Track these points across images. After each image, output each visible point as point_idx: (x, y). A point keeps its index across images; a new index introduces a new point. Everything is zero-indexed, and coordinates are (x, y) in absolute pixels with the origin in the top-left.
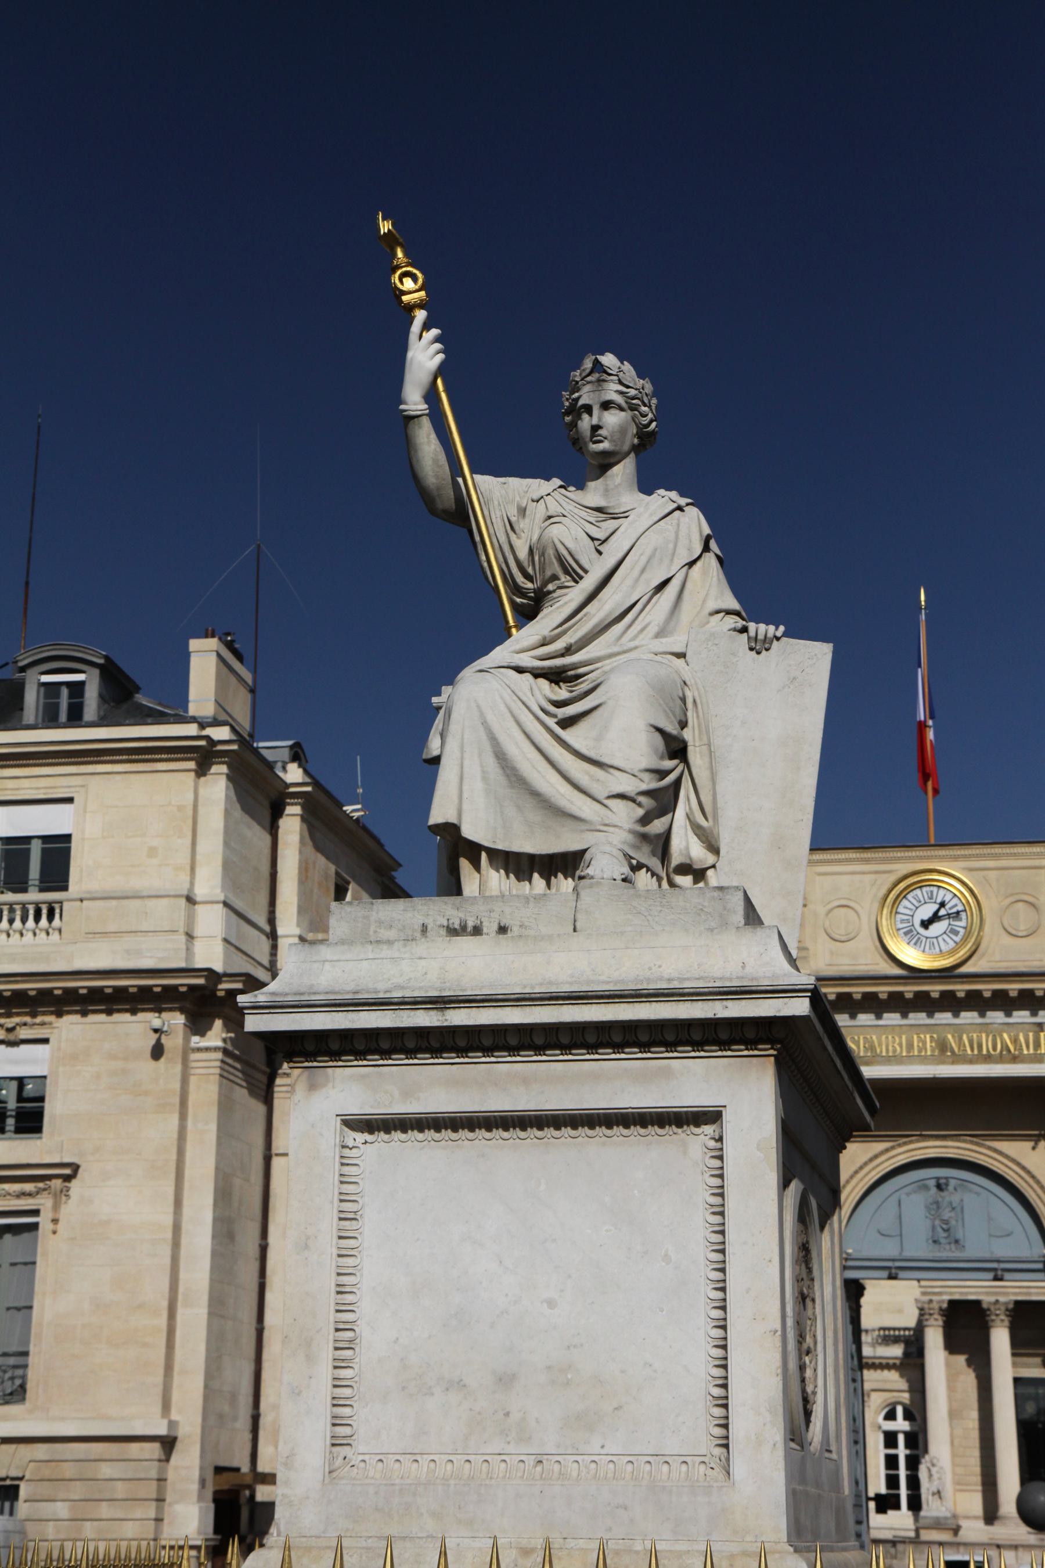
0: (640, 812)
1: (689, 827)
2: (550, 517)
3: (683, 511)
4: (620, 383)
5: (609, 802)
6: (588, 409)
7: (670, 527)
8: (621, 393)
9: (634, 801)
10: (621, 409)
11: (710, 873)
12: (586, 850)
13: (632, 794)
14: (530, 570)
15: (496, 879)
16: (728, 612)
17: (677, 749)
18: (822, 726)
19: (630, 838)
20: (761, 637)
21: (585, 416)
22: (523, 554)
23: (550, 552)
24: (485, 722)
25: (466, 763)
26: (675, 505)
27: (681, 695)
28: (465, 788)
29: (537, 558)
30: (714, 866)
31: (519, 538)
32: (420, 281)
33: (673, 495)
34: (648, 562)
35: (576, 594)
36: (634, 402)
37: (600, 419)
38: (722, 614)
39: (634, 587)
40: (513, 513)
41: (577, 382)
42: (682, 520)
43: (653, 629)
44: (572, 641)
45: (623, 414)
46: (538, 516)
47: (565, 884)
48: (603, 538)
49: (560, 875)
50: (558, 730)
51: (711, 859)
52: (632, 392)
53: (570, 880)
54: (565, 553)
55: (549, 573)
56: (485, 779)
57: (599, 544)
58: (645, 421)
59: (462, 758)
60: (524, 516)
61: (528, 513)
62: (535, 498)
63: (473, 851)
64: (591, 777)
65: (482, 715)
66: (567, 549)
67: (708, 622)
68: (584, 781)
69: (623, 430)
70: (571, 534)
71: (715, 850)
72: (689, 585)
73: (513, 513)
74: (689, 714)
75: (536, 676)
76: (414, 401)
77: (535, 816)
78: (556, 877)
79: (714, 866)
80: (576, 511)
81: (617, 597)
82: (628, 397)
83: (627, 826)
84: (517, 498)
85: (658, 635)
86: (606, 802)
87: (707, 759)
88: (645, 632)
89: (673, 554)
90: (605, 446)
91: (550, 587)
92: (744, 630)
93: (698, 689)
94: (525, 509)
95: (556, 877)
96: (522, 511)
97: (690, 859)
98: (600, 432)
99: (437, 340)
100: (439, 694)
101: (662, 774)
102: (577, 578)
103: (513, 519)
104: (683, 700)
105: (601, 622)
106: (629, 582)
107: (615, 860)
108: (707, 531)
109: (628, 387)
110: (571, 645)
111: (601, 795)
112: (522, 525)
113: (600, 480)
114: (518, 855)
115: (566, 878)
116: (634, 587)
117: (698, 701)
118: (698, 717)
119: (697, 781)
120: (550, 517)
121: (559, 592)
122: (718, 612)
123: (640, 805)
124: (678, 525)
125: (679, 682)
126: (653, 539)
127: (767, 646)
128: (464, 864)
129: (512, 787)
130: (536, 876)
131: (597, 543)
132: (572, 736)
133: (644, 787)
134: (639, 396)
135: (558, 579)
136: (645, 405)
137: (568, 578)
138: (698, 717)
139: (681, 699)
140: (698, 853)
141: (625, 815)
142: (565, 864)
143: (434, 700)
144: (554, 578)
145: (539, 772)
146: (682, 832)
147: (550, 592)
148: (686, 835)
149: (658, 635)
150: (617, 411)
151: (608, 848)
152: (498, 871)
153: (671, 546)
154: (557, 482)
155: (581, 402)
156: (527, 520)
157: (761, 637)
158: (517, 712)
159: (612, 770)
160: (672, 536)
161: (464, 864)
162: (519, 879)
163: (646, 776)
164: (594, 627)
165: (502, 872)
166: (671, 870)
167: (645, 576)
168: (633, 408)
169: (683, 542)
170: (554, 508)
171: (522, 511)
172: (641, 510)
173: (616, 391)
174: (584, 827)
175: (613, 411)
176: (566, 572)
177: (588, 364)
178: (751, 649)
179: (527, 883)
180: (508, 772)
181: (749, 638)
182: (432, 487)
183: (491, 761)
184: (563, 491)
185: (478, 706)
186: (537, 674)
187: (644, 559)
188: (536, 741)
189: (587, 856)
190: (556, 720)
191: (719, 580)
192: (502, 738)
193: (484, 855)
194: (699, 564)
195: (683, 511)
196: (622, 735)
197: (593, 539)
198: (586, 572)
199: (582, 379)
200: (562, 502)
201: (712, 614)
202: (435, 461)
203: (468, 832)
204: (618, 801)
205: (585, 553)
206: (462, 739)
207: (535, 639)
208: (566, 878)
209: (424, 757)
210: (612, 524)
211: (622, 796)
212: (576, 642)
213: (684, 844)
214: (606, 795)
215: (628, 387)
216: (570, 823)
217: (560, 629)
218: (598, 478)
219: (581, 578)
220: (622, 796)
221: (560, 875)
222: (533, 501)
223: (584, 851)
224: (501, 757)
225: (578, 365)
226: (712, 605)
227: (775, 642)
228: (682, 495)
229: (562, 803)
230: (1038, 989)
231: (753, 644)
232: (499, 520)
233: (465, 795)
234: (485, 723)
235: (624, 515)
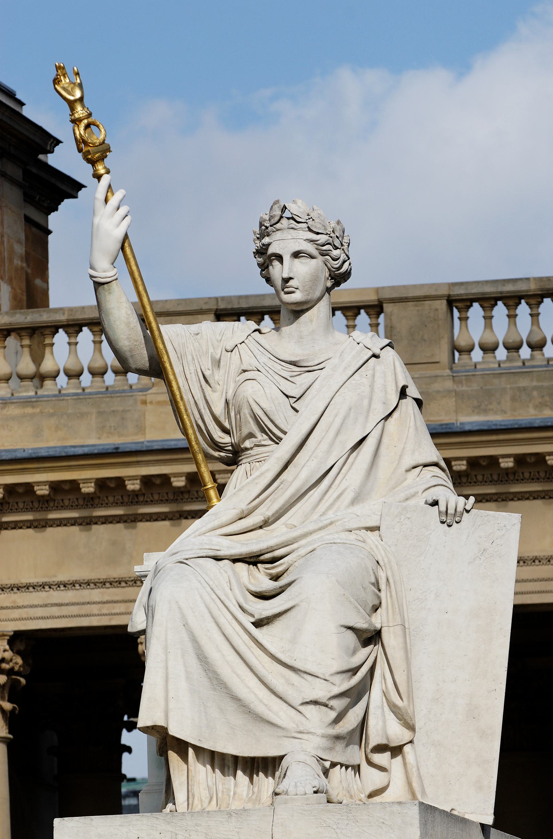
0: (333, 715)
1: (385, 704)
2: (245, 371)
4: (310, 230)
5: (301, 708)
9: (326, 706)
10: (312, 257)
11: (407, 749)
13: (324, 700)
14: (227, 425)
15: (202, 772)
17: (371, 638)
19: (324, 742)
20: (451, 511)
21: (276, 263)
22: (219, 409)
23: (246, 411)
24: (187, 624)
25: (170, 663)
26: (370, 353)
28: (171, 687)
29: (232, 414)
30: (411, 742)
31: (214, 391)
34: (342, 424)
36: (324, 248)
37: (290, 270)
38: (421, 467)
39: (329, 452)
40: (207, 366)
41: (267, 228)
42: (378, 368)
43: (349, 496)
46: (233, 367)
47: (265, 783)
48: (298, 397)
49: (261, 774)
50: (252, 628)
51: (406, 735)
52: (323, 239)
53: (270, 778)
55: (245, 432)
56: (188, 678)
57: (294, 401)
58: (336, 264)
59: (166, 661)
60: (219, 366)
61: (222, 364)
62: (229, 348)
63: (181, 747)
65: (183, 617)
67: (405, 479)
68: (280, 687)
69: (314, 279)
70: (264, 394)
71: (412, 728)
72: (385, 440)
73: (207, 366)
74: (383, 595)
77: (237, 719)
78: (258, 775)
79: (411, 742)
80: (270, 364)
81: (313, 464)
83: (320, 731)
84: (211, 350)
85: (354, 501)
86: (301, 708)
87: (401, 640)
88: (341, 499)
89: (368, 411)
90: (297, 297)
93: (391, 568)
95: (258, 775)
96: (217, 363)
97: (388, 739)
98: (291, 283)
100: (141, 563)
101: (354, 671)
102: (277, 440)
103: (207, 373)
105: (298, 491)
106: (324, 446)
107: (309, 769)
109: (318, 233)
110: (269, 519)
111: (296, 702)
112: (216, 377)
113: (294, 325)
114: (223, 756)
116: (329, 452)
117: (391, 581)
118: (391, 596)
119: (391, 662)
120: (245, 371)
121: (257, 450)
123: (331, 708)
124: (373, 376)
125: (371, 565)
126: (347, 397)
127: (457, 519)
128: (173, 756)
129: (215, 690)
130: (239, 773)
133: (337, 690)
134: (331, 241)
135: (255, 437)
136: (336, 248)
137: (265, 437)
138: (391, 596)
139: (373, 584)
140: (396, 733)
141: (317, 720)
142: (268, 765)
144: (251, 435)
145: (238, 675)
146: (379, 712)
147: (247, 449)
148: (383, 715)
149: (354, 501)
150: (309, 260)
151: (302, 757)
152: (205, 766)
153: (366, 402)
155: (271, 250)
156: (222, 371)
157: (451, 511)
158: (212, 606)
159: (305, 676)
161: (173, 756)
162: (223, 773)
163: (337, 679)
164: (291, 497)
165: (209, 767)
166: (368, 751)
167: (341, 438)
168: (323, 254)
169: (378, 395)
170: (249, 361)
171: (217, 363)
172: (334, 361)
174: (281, 733)
175: (303, 260)
176: (263, 431)
178: (443, 522)
179: (232, 778)
180: (210, 675)
181: (440, 512)
182: (125, 349)
183: (193, 662)
185: (179, 608)
188: (235, 645)
189: (284, 763)
191: (416, 429)
192: (204, 642)
194: (396, 415)
196: (316, 638)
198: (285, 433)
199: (271, 226)
200: (256, 352)
201: (408, 471)
202: (128, 324)
203: (174, 731)
204: (311, 707)
205: (281, 414)
206: (166, 640)
207: (233, 513)
208: (267, 777)
210: (307, 378)
211: (315, 703)
212: (273, 515)
213: (384, 727)
214: (300, 702)
215: (318, 233)
216: (267, 727)
217: (257, 501)
218: (292, 324)
219: (280, 439)
220: (315, 703)
221: (261, 774)
223: (282, 758)
224: (203, 659)
226: (409, 461)
227: (465, 514)
229: (260, 709)
231: (444, 518)
232: (193, 375)
233: (171, 695)
234: (186, 625)
235: (319, 367)
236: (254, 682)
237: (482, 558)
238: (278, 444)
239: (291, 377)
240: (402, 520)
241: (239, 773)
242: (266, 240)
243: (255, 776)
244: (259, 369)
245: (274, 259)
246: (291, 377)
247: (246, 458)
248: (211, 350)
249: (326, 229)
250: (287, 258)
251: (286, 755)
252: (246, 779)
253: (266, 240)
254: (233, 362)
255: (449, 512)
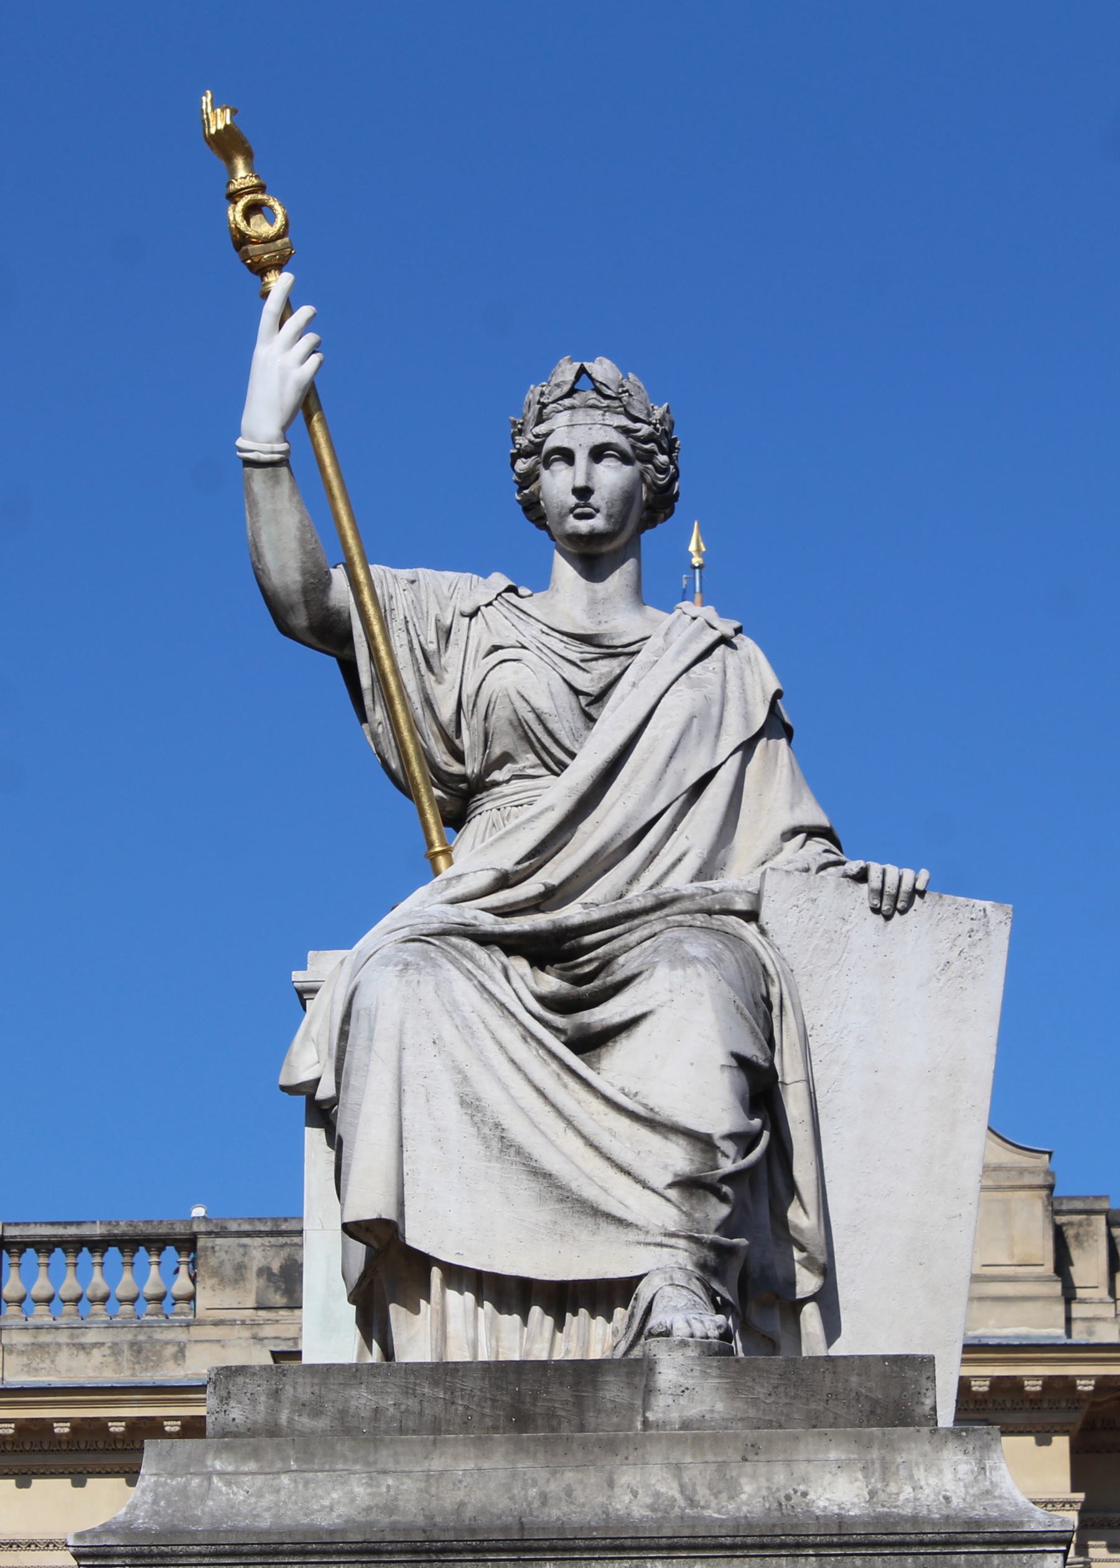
2: (496, 648)
3: (733, 646)
6: (567, 456)
7: (710, 675)
8: (625, 431)
12: (640, 1278)
16: (813, 832)
18: (993, 1050)
20: (890, 888)
27: (764, 993)
32: (280, 220)
33: (709, 613)
35: (558, 794)
37: (589, 476)
44: (555, 881)
45: (627, 469)
49: (583, 1312)
54: (530, 717)
55: (497, 751)
62: (468, 608)
63: (420, 1264)
64: (612, 1133)
66: (533, 710)
67: (781, 850)
75: (509, 951)
76: (261, 427)
78: (575, 1314)
82: (638, 439)
91: (496, 776)
92: (862, 877)
94: (449, 632)
95: (575, 1314)
99: (309, 326)
100: (303, 967)
104: (767, 1001)
108: (773, 685)
109: (636, 420)
115: (593, 1317)
120: (496, 648)
121: (516, 785)
122: (794, 832)
130: (536, 1311)
131: (583, 700)
132: (617, 1068)
143: (297, 976)
144: (506, 758)
147: (496, 784)
153: (715, 711)
154: (500, 581)
155: (551, 443)
157: (890, 888)
160: (715, 690)
167: (676, 765)
173: (616, 428)
174: (632, 1235)
177: (566, 372)
184: (511, 597)
186: (511, 945)
187: (672, 735)
190: (563, 1038)
193: (436, 1274)
195: (733, 646)
197: (577, 692)
198: (572, 755)
205: (562, 716)
209: (283, 1080)
210: (606, 668)
215: (636, 420)
216: (612, 1229)
219: (563, 766)
221: (583, 1312)
222: (463, 615)
225: (544, 373)
228: (722, 613)
230: (1082, 1377)
236: (574, 1144)
237: (943, 979)
238: (558, 775)
239: (583, 661)
240: (801, 902)
241: (536, 1311)
242: (542, 429)
243: (568, 1315)
244: (526, 645)
245: (556, 460)
246: (583, 661)
247: (493, 800)
248: (434, 612)
249: (649, 415)
250: (581, 458)
251: (646, 1275)
252: (549, 1321)
253: (542, 429)
254: (480, 634)
255: (887, 889)
